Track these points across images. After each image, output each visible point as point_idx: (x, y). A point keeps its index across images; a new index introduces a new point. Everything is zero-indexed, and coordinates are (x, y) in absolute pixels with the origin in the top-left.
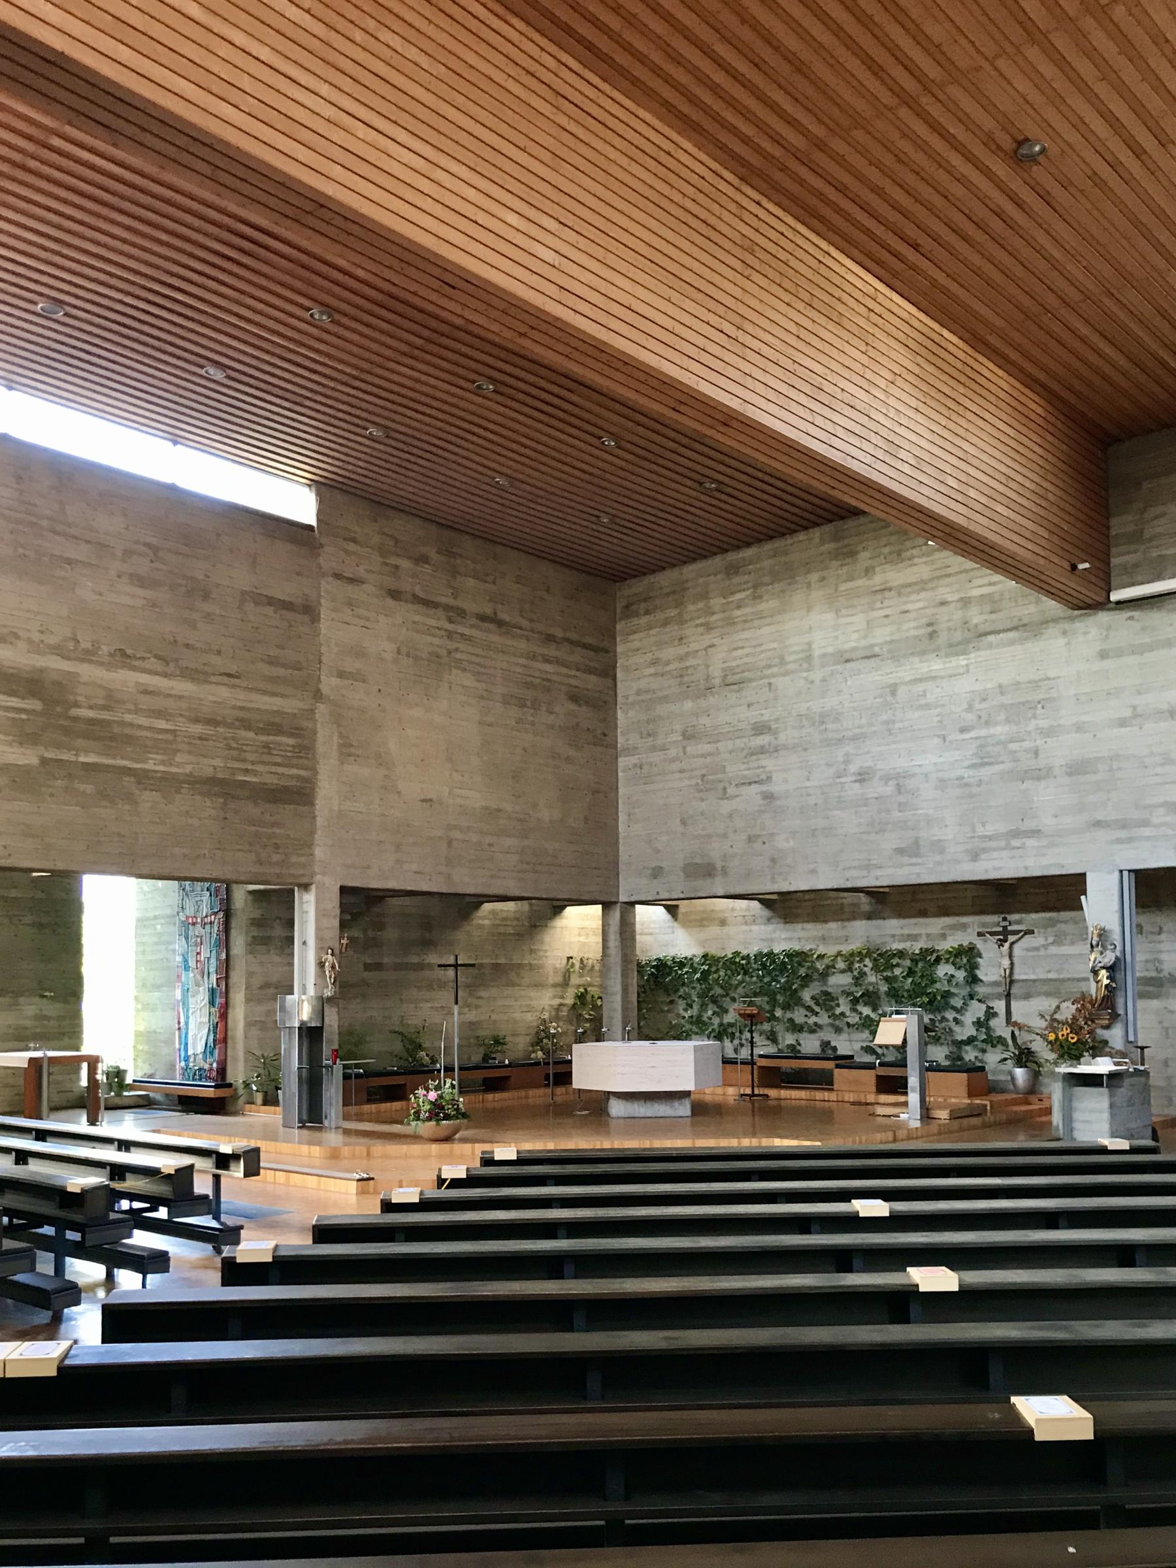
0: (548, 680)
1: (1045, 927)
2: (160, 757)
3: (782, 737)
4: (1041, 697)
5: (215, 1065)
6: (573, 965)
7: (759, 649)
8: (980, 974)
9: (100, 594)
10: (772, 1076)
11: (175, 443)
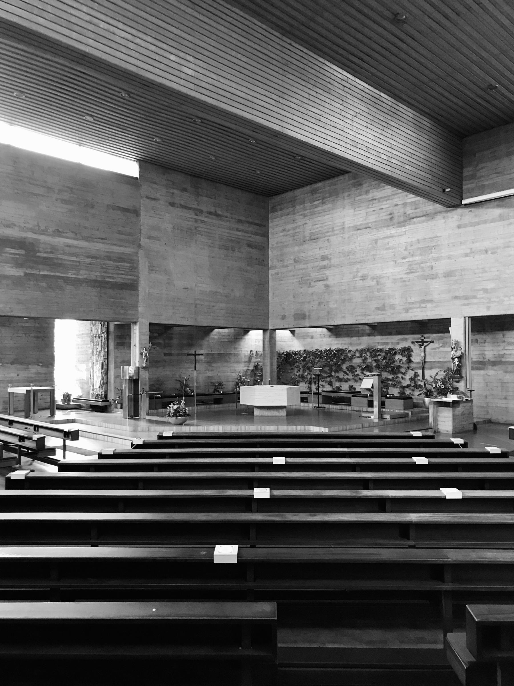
0: (239, 238)
1: (439, 340)
2: (73, 272)
3: (333, 261)
4: (434, 244)
5: (103, 393)
6: (253, 354)
7: (324, 225)
8: (412, 359)
9: (49, 207)
10: (329, 400)
11: (80, 146)
